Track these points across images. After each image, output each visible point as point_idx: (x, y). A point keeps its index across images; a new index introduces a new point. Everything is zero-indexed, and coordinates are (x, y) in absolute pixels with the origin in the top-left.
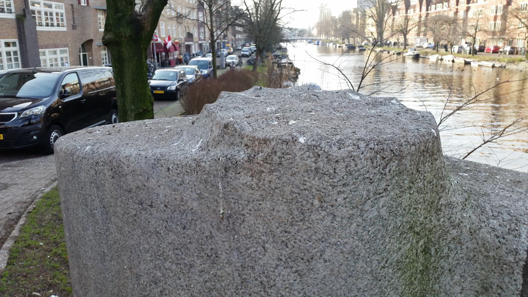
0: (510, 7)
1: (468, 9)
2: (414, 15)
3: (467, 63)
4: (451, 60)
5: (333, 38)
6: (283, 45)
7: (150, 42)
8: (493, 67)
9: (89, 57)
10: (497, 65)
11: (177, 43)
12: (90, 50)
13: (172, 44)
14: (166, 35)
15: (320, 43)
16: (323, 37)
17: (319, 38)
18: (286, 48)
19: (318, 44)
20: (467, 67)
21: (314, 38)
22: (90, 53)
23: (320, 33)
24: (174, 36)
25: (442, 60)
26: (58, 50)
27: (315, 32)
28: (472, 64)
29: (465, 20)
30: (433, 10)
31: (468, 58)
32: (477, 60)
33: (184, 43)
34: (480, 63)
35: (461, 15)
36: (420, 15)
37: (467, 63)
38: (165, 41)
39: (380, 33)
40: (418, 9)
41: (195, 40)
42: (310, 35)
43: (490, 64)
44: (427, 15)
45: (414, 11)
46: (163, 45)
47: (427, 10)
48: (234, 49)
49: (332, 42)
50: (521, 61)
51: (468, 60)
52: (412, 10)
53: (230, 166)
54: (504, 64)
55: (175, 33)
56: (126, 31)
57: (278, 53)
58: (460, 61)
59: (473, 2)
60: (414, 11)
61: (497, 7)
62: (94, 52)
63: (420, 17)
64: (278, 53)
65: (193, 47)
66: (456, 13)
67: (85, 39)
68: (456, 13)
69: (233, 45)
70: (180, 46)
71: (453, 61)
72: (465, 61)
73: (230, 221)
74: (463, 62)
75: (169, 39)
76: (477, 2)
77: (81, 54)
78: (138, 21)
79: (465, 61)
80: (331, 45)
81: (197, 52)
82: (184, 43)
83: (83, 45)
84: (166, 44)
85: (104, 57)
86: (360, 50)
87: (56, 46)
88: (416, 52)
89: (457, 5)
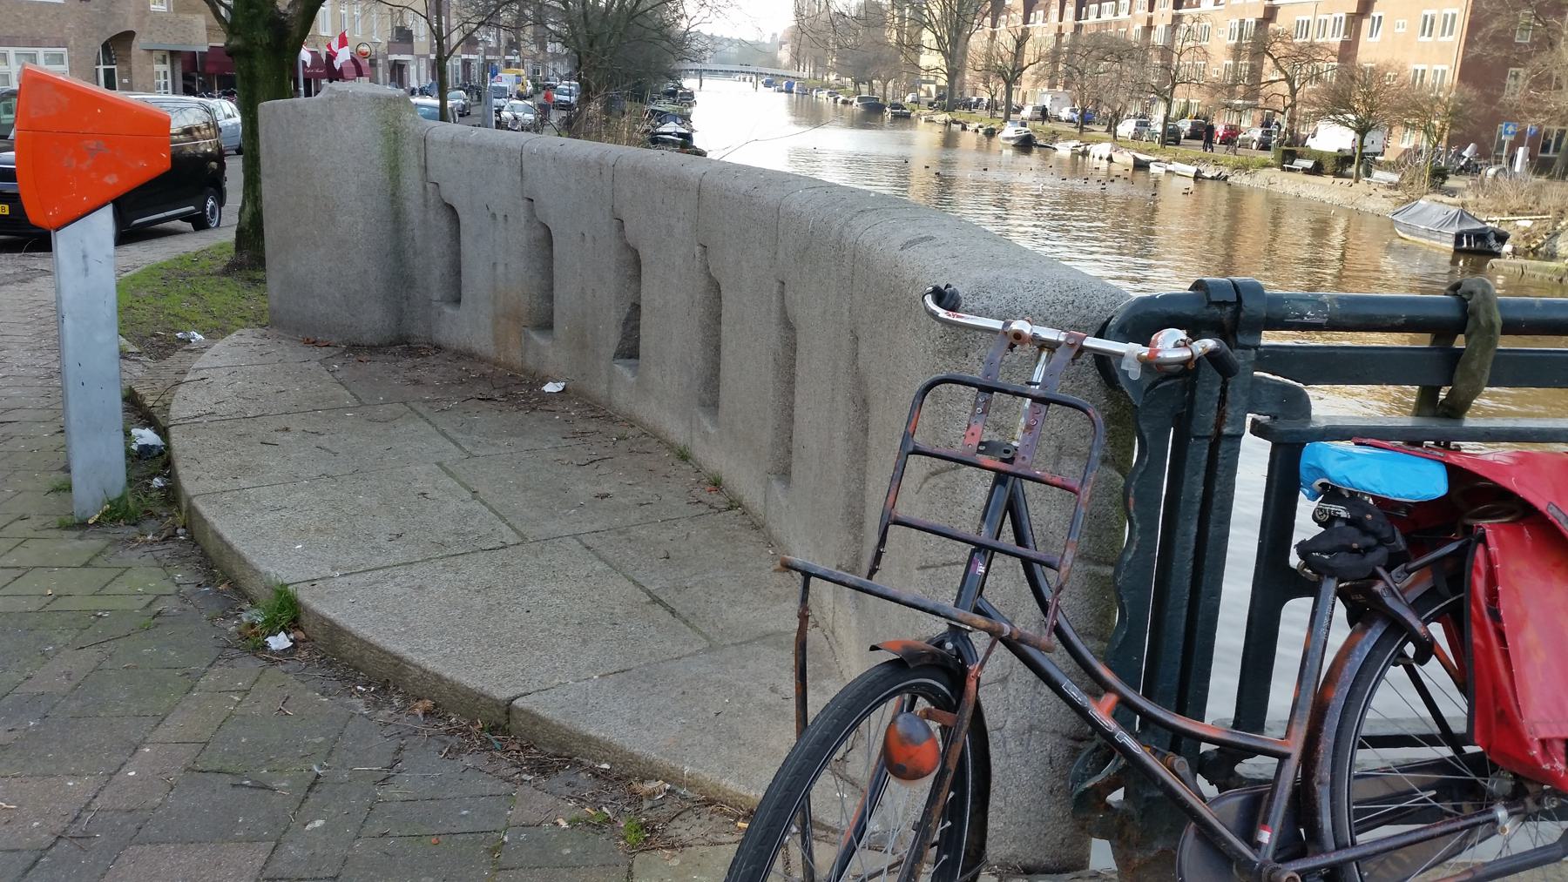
0: (1271, 25)
1: (1177, 19)
2: (1044, 29)
3: (1141, 166)
4: (1106, 156)
5: (832, 77)
6: (689, 83)
7: (1185, 363)
8: (1198, 177)
9: (121, 77)
10: (1209, 172)
11: (364, 54)
12: (125, 59)
13: (354, 60)
14: (334, 31)
15: (795, 89)
16: (806, 72)
17: (794, 73)
18: (691, 95)
19: (789, 91)
20: (1141, 174)
21: (779, 72)
22: (125, 69)
23: (797, 58)
24: (356, 34)
25: (1085, 154)
26: (41, 52)
27: (784, 55)
28: (1153, 168)
29: (1167, 51)
30: (1092, 18)
31: (1148, 152)
32: (1167, 158)
33: (385, 57)
34: (1170, 167)
35: (1158, 37)
36: (1060, 28)
37: (1141, 166)
38: (329, 46)
39: (954, 73)
40: (1055, 11)
41: (416, 52)
42: (774, 63)
43: (1192, 170)
44: (1078, 28)
45: (1046, 16)
46: (324, 58)
47: (1078, 16)
48: (536, 86)
49: (828, 86)
50: (1266, 165)
51: (1142, 157)
52: (1041, 13)
53: (331, 99)
54: (1226, 171)
55: (359, 25)
56: (264, 37)
57: (664, 106)
58: (1125, 159)
59: (1190, 6)
60: (1046, 16)
61: (1242, 22)
62: (135, 66)
63: (1060, 35)
64: (664, 106)
65: (413, 68)
66: (1149, 28)
67: (113, 30)
68: (1149, 28)
69: (536, 72)
70: (373, 64)
71: (1110, 159)
72: (1136, 159)
73: (331, 117)
74: (1131, 161)
75: (343, 42)
76: (1198, 5)
77: (101, 68)
78: (283, 22)
79: (1136, 159)
80: (824, 95)
81: (423, 84)
82: (385, 57)
83: (106, 47)
84: (331, 57)
85: (162, 81)
86: (896, 117)
87: (36, 43)
88: (1024, 131)
89: (1151, 9)
